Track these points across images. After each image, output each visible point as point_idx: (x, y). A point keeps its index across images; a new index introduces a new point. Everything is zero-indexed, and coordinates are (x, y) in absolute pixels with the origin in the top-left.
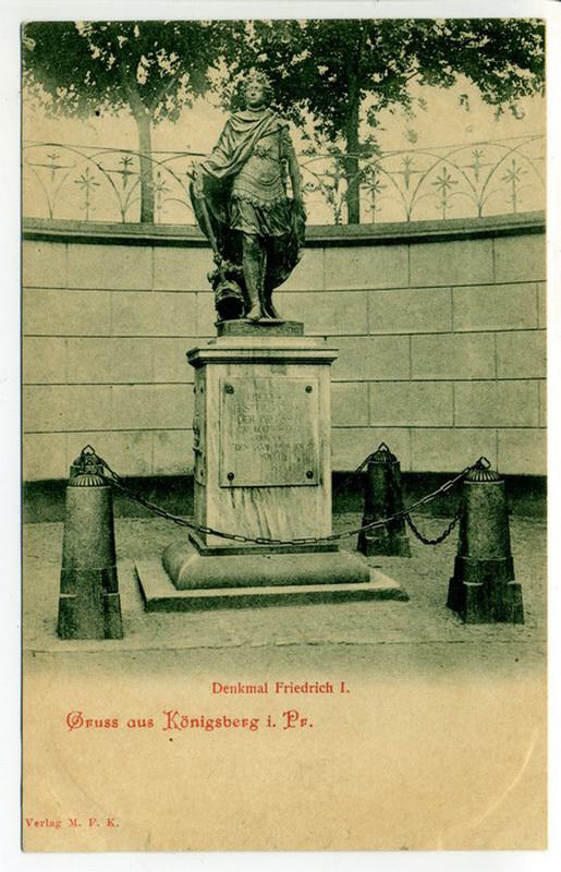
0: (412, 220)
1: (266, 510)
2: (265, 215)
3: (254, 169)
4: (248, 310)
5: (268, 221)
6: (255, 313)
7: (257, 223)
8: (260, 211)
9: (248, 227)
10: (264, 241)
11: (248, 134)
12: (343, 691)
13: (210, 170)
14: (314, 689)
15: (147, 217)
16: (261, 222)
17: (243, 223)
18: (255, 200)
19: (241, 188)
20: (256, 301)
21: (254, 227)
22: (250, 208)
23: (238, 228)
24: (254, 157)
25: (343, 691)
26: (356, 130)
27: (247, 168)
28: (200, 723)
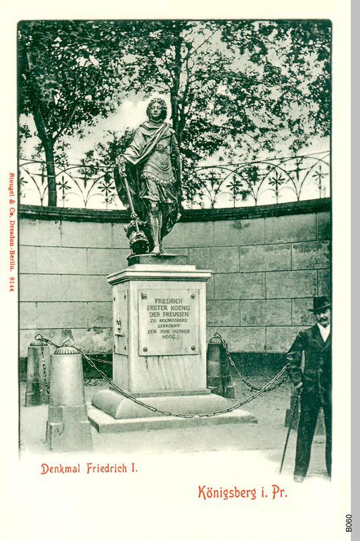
0: (215, 207)
1: (159, 375)
2: (163, 189)
3: (157, 160)
4: (152, 249)
5: (165, 193)
6: (156, 250)
7: (158, 193)
8: (160, 186)
9: (153, 197)
10: (162, 206)
11: (153, 137)
12: (263, 496)
13: (129, 159)
14: (113, 469)
15: (52, 201)
16: (161, 192)
17: (149, 193)
18: (158, 179)
19: (149, 171)
20: (156, 242)
21: (156, 197)
22: (154, 184)
23: (146, 197)
24: (156, 152)
25: (263, 496)
26: (209, 220)
27: (152, 159)
28: (220, 494)
